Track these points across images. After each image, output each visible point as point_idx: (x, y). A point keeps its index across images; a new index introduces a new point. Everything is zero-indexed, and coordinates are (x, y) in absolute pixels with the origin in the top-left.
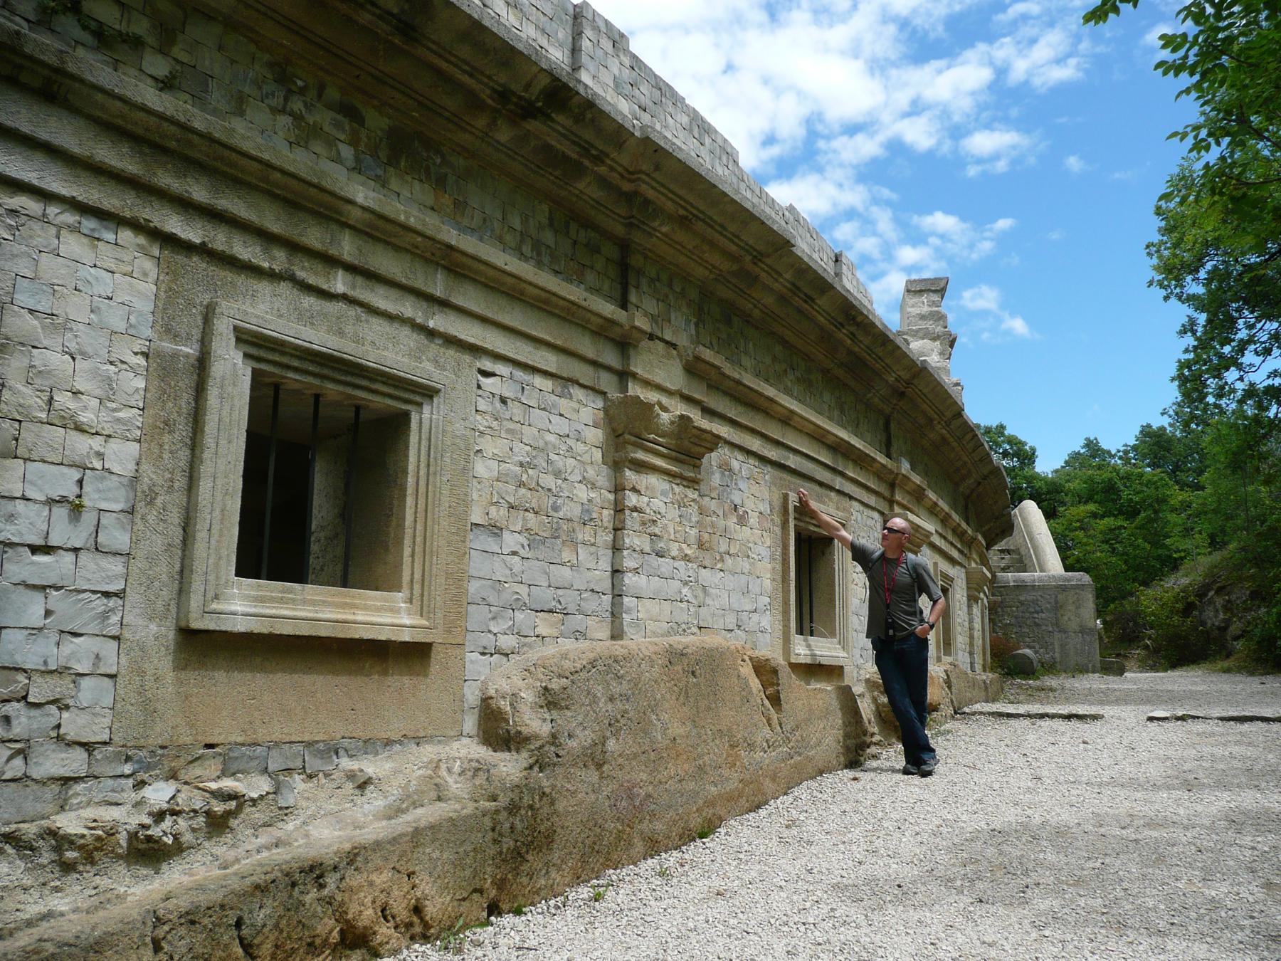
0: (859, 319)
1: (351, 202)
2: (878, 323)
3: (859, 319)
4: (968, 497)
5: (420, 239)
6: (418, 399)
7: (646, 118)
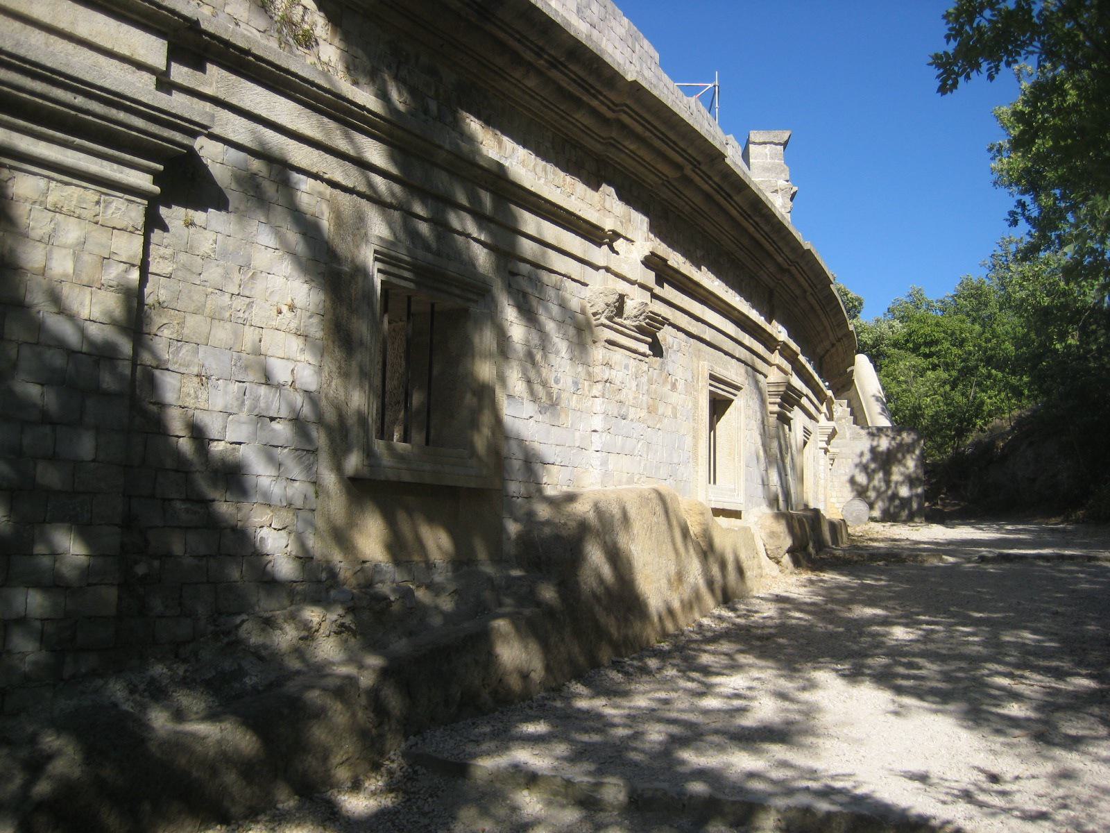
0: (764, 211)
1: (440, 147)
2: (777, 214)
3: (764, 211)
4: (823, 356)
5: (480, 172)
6: (475, 298)
7: (595, 33)
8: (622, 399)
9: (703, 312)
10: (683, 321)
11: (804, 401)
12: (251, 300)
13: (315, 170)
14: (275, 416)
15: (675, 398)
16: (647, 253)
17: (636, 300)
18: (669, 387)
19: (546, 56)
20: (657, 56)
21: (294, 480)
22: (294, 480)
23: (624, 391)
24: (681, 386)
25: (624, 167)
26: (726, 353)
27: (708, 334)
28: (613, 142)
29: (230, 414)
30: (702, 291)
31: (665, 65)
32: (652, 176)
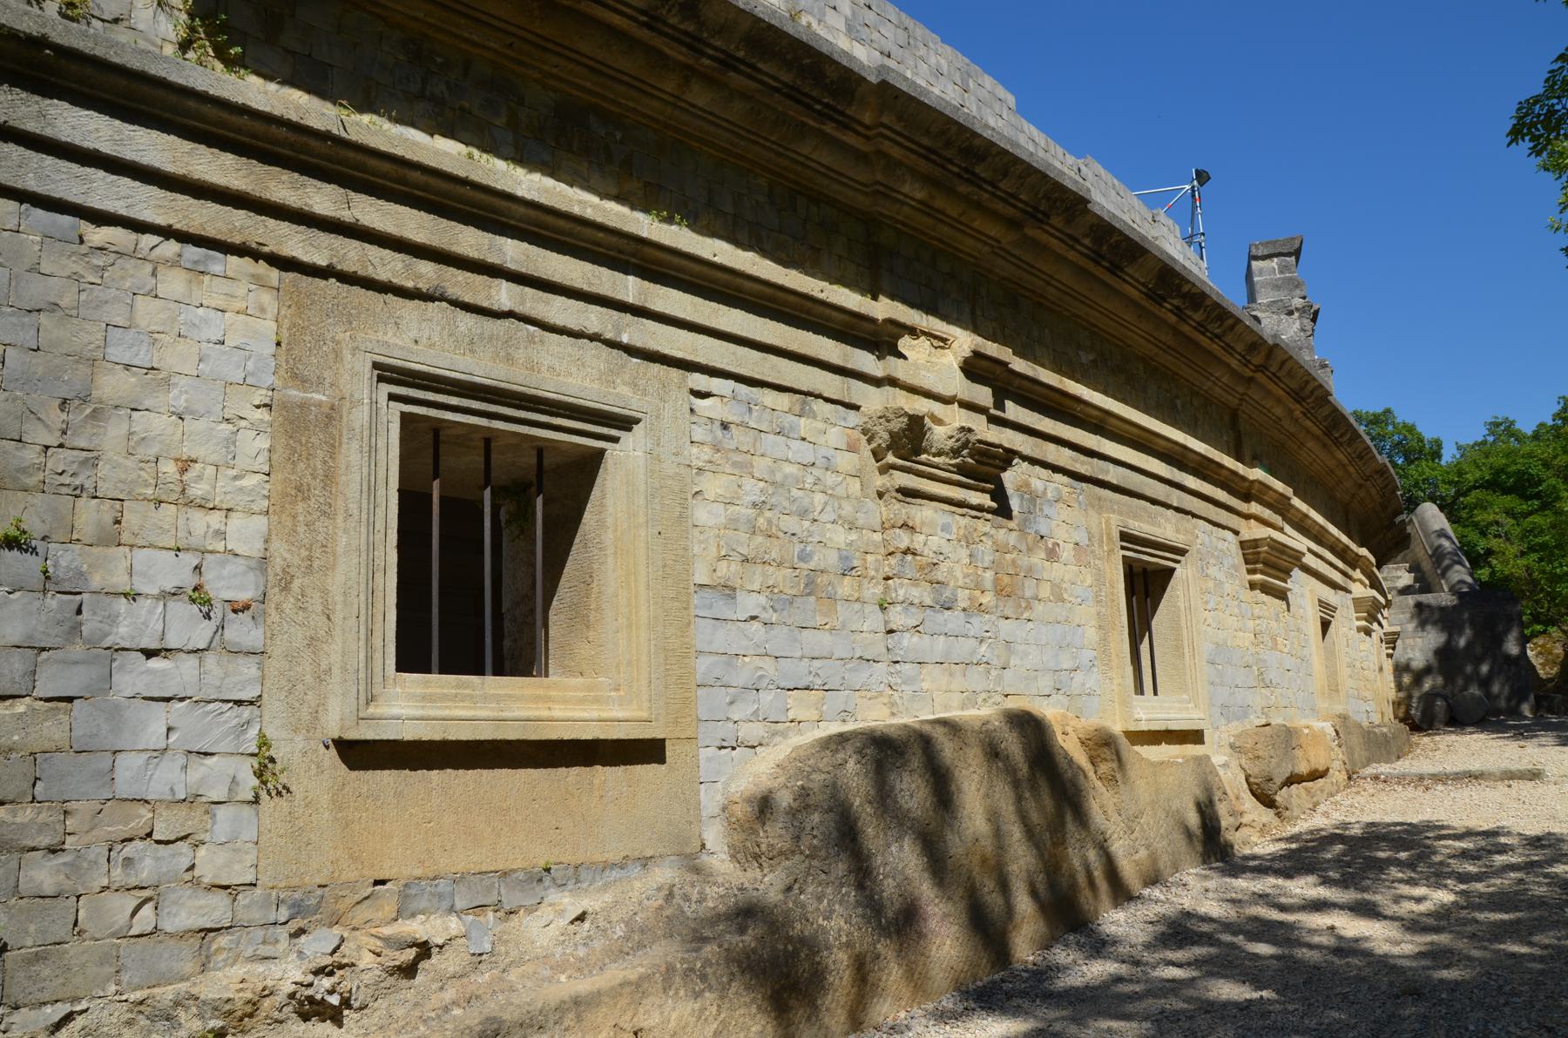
8: (940, 578)
9: (42, 115)
10: (1053, 453)
11: (1309, 560)
12: (95, 454)
13: (237, 239)
14: (154, 645)
15: (1055, 571)
16: (968, 354)
17: (947, 426)
18: (1043, 555)
19: (711, 52)
20: (1011, 100)
21: (206, 754)
22: (206, 754)
23: (943, 567)
24: (1066, 552)
25: (915, 229)
26: (1154, 502)
27: (1114, 474)
28: (882, 189)
29: (44, 649)
30: (207, 109)
31: (1023, 110)
32: (971, 242)
